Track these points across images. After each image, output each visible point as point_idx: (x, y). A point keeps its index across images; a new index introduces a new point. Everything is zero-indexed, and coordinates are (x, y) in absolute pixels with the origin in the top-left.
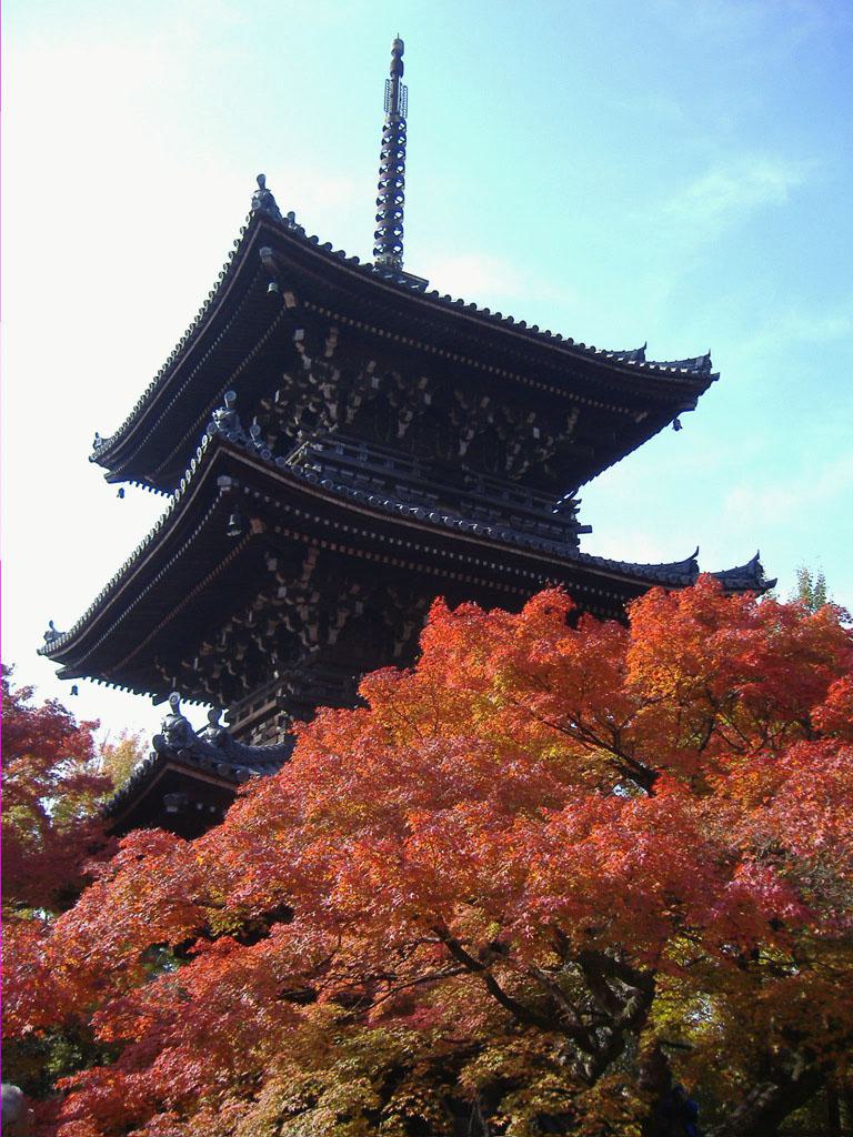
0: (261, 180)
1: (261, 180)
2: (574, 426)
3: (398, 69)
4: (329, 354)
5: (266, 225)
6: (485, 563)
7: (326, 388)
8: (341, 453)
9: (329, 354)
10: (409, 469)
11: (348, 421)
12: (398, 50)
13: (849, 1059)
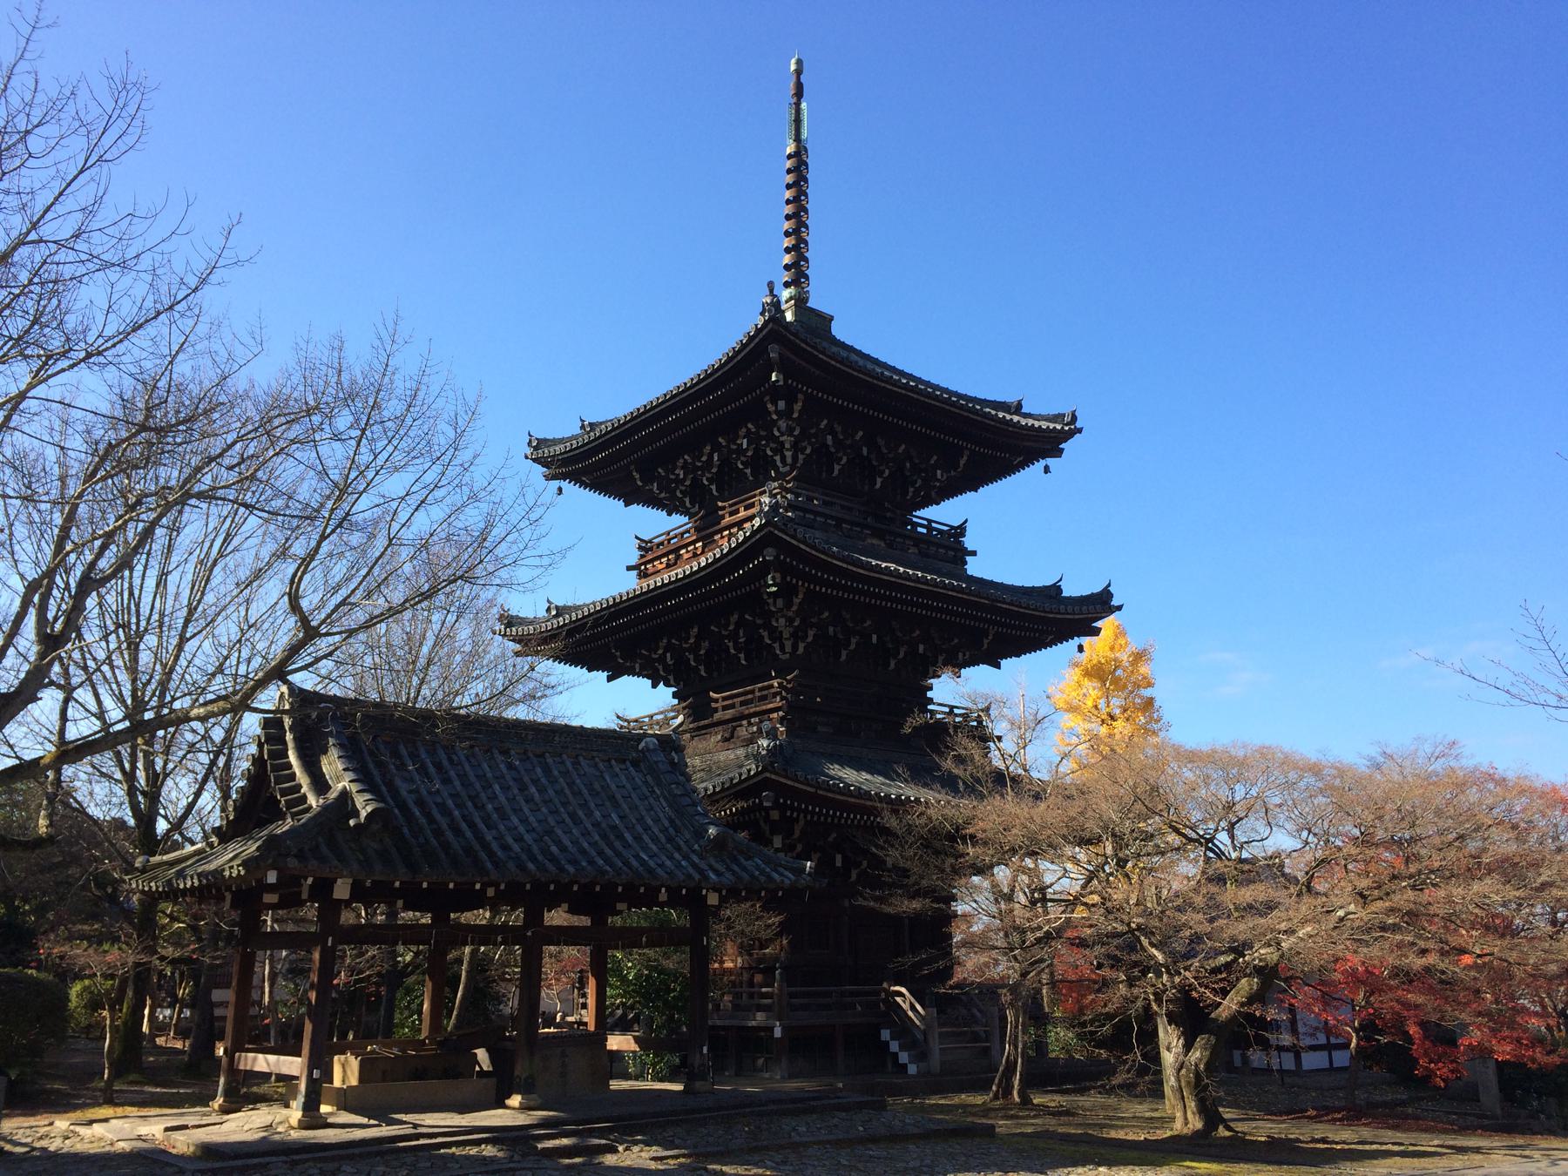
4: (795, 415)
9: (795, 415)
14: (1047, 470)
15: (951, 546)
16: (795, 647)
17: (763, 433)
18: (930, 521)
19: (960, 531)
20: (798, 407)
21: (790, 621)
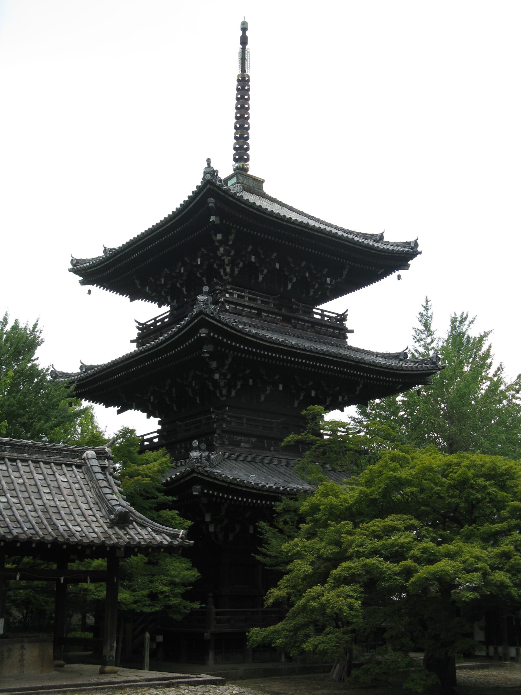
0: (209, 161)
1: (209, 161)
2: (346, 274)
3: (244, 41)
4: (230, 243)
5: (212, 187)
6: (314, 363)
7: (227, 259)
8: (237, 297)
9: (230, 243)
10: (268, 303)
11: (235, 274)
12: (244, 29)
13: (2, 406)
14: (399, 277)
15: (338, 327)
16: (229, 392)
17: (211, 254)
18: (323, 311)
19: (343, 317)
20: (232, 237)
21: (223, 375)
